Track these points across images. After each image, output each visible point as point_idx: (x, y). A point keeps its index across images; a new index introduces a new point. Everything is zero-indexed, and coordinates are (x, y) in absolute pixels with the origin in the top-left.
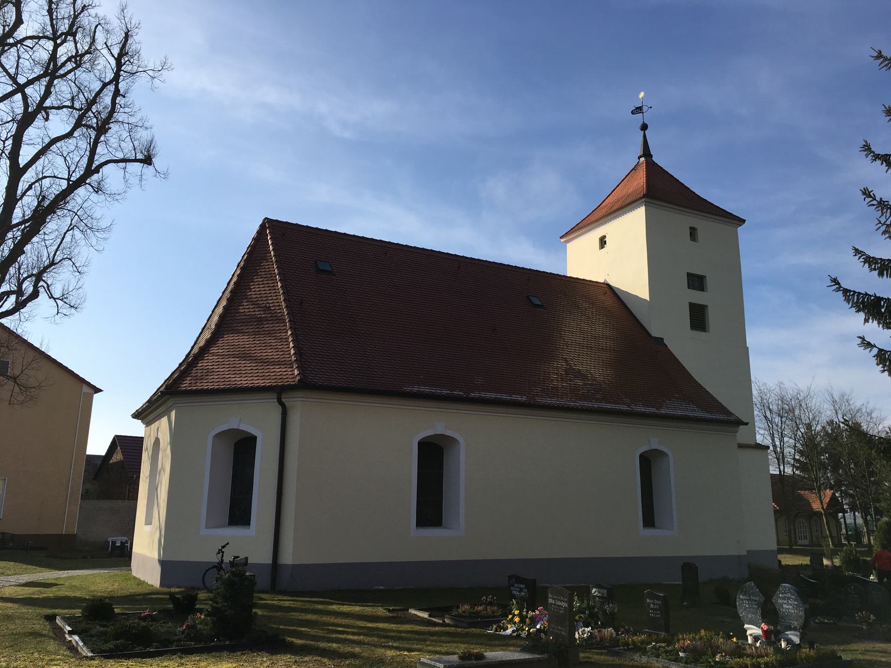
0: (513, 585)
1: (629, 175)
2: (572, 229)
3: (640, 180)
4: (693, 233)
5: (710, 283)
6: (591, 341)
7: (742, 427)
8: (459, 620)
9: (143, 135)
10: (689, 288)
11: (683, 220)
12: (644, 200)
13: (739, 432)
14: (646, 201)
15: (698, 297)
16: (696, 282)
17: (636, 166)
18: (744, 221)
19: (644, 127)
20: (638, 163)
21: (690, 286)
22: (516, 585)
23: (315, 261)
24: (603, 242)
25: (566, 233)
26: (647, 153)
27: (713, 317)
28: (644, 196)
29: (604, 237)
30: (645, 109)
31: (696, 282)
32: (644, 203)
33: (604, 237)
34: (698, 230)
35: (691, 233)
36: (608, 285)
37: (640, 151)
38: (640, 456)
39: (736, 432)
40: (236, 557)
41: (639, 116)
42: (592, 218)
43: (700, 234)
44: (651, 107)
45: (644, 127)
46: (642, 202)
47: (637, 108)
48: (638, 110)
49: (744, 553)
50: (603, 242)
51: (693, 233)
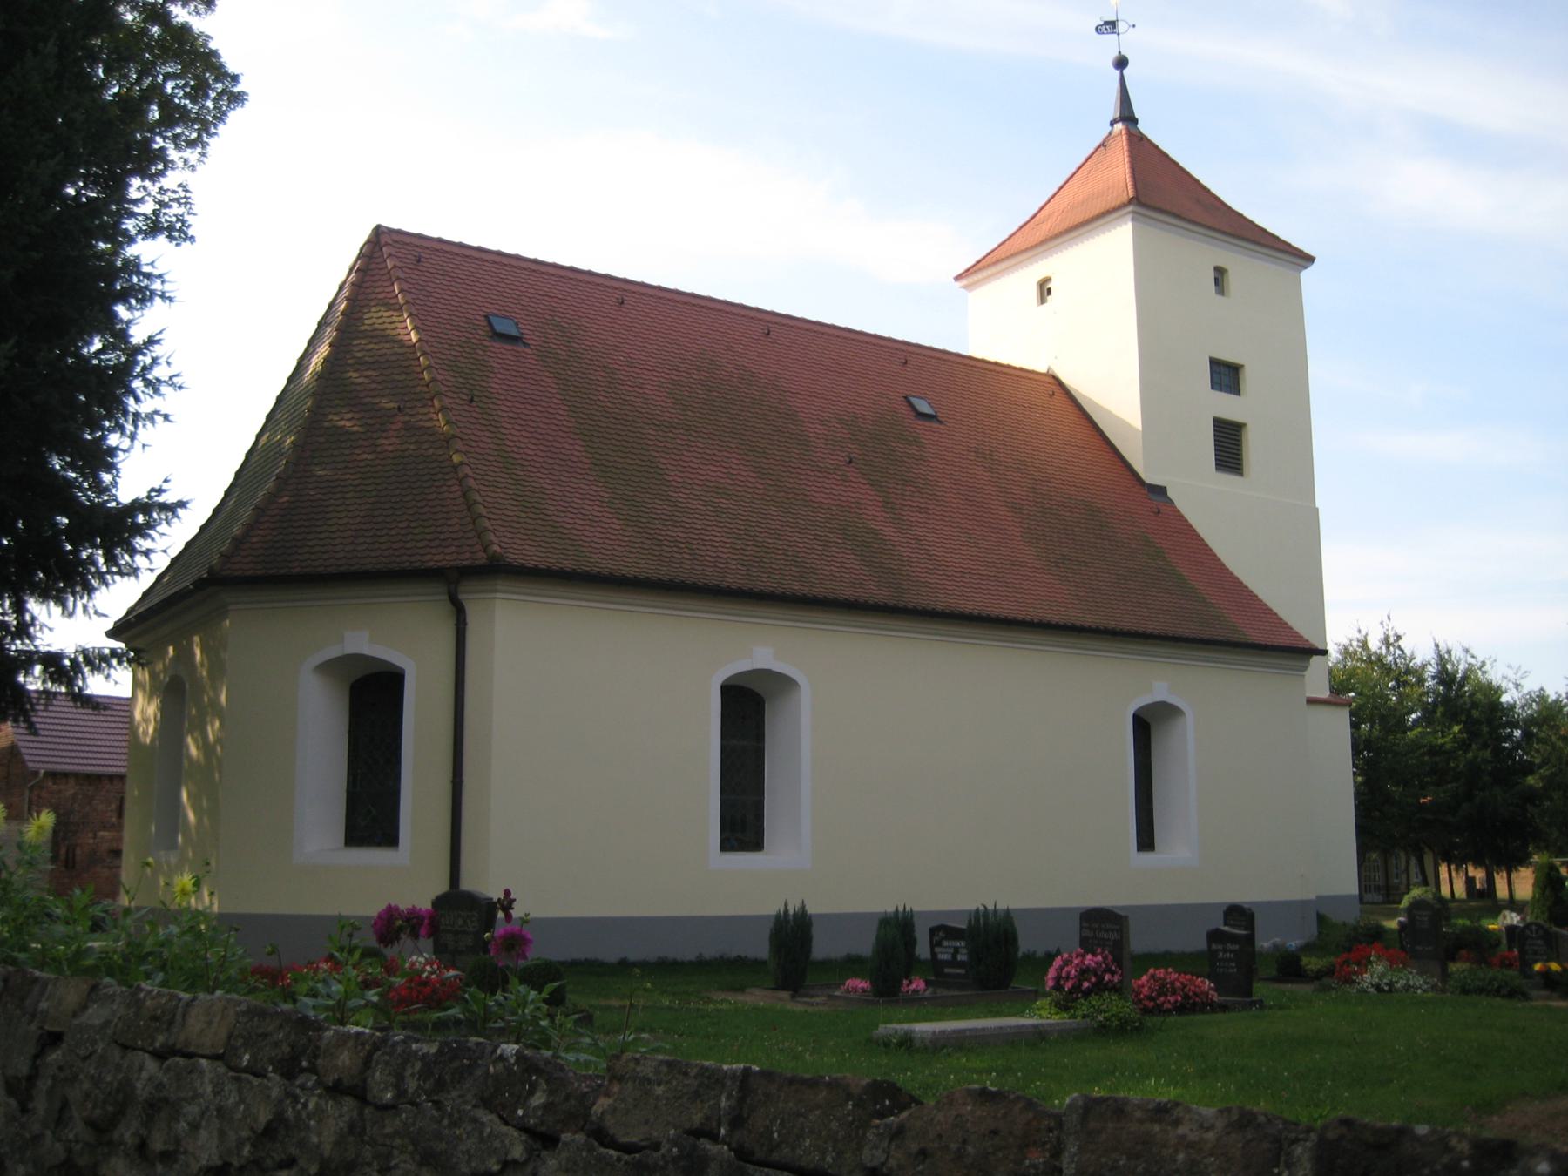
0: (939, 944)
1: (1093, 158)
2: (978, 262)
3: (1118, 173)
4: (1220, 273)
5: (1248, 379)
6: (874, 513)
7: (1315, 659)
8: (76, 674)
9: (186, 10)
10: (1213, 388)
11: (1202, 254)
12: (1131, 208)
13: (1309, 669)
14: (1133, 212)
15: (1228, 407)
16: (1226, 375)
17: (1105, 140)
18: (1310, 259)
19: (1121, 63)
20: (1110, 134)
21: (1216, 385)
22: (945, 943)
23: (485, 316)
24: (1044, 290)
25: (967, 270)
26: (1127, 116)
27: (1254, 447)
28: (1131, 201)
29: (1047, 280)
30: (1121, 27)
31: (1226, 375)
32: (1130, 216)
33: (1047, 280)
34: (1230, 272)
35: (1216, 279)
36: (1055, 378)
37: (1111, 109)
38: (723, 687)
39: (1305, 668)
40: (527, 915)
41: (1110, 39)
42: (1019, 242)
43: (1232, 280)
44: (1134, 26)
45: (1121, 63)
46: (1126, 214)
47: (1106, 23)
48: (1110, 26)
49: (1312, 896)
50: (1044, 290)
51: (1220, 273)
